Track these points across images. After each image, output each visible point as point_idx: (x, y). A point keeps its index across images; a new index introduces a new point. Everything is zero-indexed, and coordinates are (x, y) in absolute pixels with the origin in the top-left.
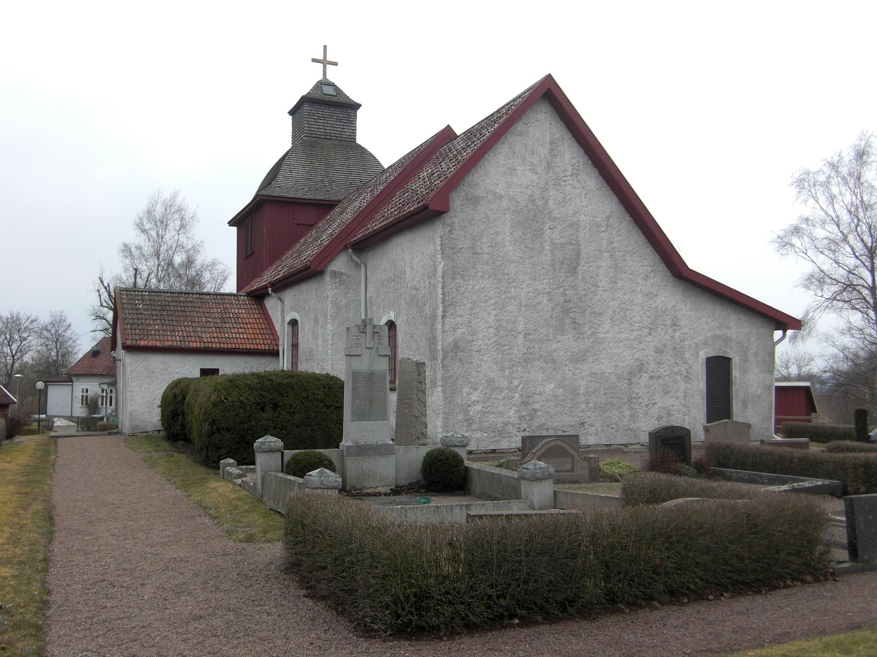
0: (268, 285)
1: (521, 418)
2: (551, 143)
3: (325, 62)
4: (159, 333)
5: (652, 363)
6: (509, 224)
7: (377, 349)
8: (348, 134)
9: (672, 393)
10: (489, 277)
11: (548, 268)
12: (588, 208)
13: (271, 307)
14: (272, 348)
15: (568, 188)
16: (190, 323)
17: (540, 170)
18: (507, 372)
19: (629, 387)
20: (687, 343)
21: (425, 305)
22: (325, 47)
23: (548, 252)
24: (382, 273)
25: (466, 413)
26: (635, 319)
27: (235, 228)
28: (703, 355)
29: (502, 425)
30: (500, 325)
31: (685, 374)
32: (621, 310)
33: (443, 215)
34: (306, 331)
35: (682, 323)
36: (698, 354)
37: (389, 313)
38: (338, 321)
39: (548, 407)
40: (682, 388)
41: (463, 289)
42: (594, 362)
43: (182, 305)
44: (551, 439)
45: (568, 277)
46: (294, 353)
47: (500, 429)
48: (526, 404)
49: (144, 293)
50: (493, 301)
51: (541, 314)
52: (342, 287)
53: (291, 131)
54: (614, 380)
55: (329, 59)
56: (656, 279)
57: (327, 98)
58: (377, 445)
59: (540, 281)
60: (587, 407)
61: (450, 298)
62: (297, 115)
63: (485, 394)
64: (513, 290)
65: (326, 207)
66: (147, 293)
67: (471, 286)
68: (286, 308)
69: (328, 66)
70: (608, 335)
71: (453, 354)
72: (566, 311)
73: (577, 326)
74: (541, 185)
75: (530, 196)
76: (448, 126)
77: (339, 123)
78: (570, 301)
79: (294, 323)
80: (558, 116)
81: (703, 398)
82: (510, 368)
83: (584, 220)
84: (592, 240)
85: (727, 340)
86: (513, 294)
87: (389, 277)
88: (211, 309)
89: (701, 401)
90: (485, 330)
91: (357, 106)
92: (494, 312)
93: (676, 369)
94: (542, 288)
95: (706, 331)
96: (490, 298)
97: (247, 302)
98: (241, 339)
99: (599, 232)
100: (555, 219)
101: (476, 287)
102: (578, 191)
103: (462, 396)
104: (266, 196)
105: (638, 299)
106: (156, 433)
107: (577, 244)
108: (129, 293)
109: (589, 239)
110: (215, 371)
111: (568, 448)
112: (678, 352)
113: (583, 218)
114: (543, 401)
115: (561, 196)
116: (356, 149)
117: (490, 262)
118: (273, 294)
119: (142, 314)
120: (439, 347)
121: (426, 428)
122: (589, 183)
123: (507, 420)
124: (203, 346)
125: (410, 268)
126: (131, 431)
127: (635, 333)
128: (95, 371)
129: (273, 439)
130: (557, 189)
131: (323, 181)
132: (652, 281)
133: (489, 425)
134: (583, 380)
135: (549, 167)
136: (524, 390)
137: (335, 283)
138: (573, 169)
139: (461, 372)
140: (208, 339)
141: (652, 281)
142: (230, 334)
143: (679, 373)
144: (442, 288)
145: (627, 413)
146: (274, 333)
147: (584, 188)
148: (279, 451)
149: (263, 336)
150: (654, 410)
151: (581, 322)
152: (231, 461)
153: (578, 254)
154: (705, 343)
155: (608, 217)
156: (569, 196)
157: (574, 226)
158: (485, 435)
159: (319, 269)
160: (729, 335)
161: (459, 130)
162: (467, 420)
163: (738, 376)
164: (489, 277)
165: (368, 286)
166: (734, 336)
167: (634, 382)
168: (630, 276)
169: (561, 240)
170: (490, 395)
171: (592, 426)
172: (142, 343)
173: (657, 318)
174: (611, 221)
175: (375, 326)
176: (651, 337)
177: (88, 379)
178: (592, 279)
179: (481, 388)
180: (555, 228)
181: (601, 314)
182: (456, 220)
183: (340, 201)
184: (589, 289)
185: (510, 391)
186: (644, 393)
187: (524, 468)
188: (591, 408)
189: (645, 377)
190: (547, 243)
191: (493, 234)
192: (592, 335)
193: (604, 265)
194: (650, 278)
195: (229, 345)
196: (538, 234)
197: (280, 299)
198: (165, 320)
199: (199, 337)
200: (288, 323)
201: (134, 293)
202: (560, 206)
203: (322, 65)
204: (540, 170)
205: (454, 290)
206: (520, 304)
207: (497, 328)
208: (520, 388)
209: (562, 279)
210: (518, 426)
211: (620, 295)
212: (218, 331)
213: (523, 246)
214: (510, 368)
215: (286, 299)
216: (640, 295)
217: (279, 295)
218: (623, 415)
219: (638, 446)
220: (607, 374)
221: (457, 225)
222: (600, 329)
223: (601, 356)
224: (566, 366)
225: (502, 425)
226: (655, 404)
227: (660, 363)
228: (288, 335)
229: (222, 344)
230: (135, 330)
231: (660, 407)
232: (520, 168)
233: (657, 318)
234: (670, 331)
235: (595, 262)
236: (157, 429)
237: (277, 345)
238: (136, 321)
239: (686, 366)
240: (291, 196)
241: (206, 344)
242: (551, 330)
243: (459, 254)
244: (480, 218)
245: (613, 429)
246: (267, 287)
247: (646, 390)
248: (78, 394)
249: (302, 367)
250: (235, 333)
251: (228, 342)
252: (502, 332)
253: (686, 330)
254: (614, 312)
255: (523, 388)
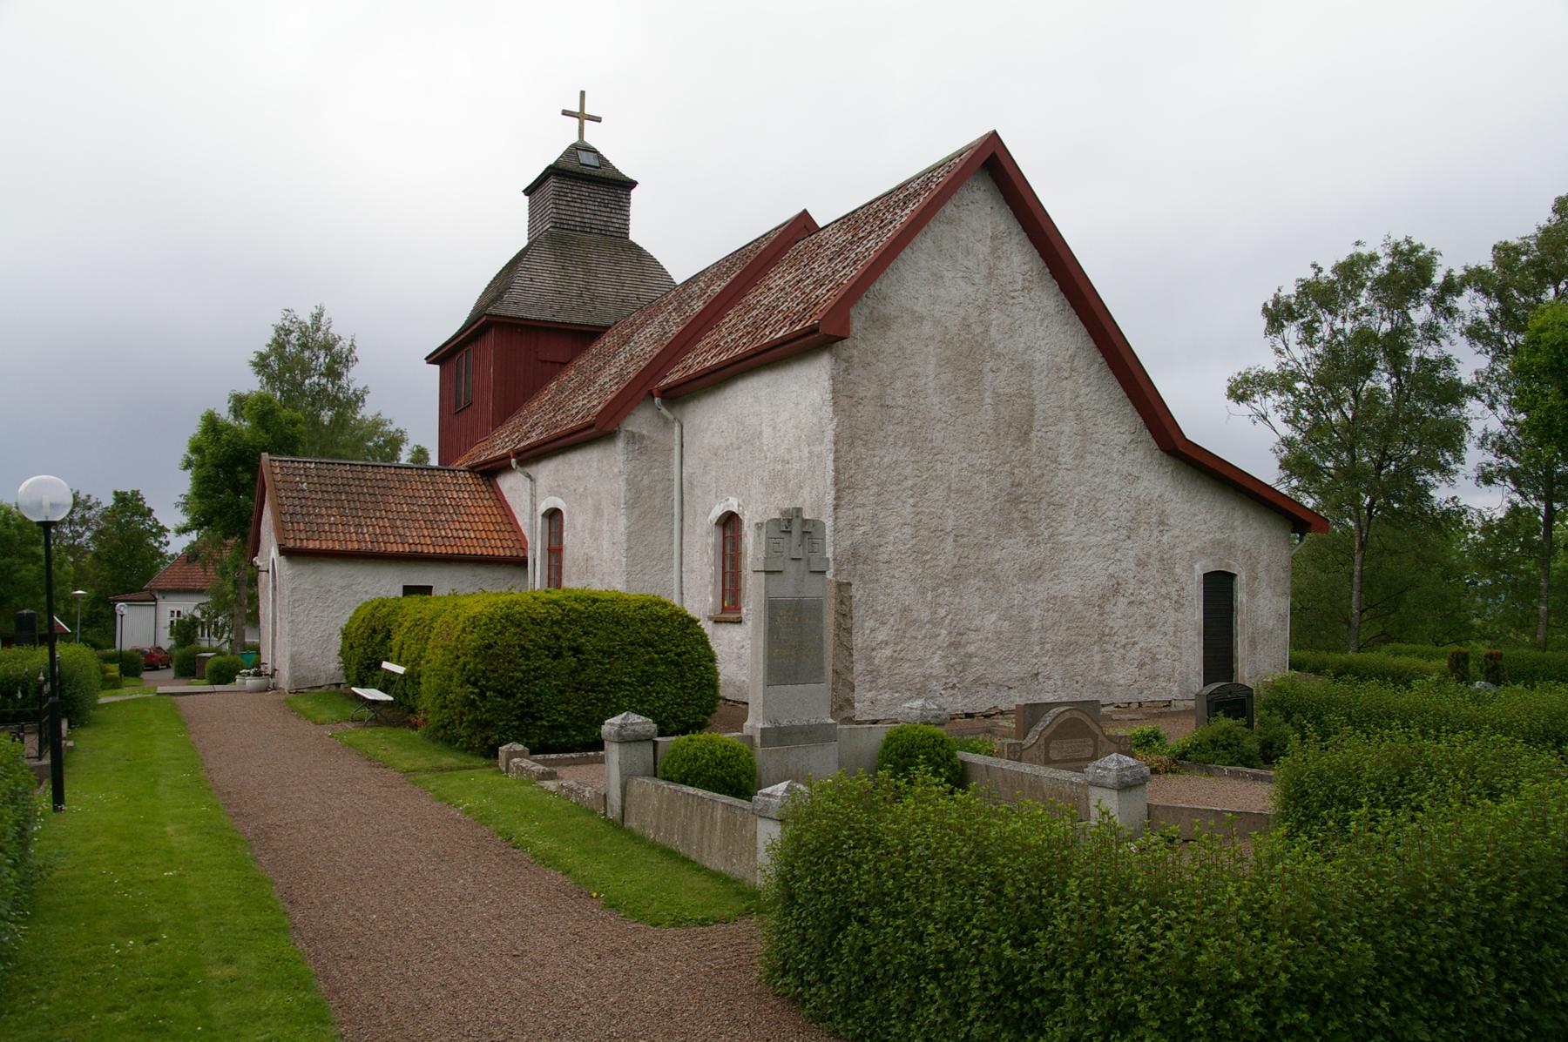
0: (511, 454)
1: (949, 667)
2: (993, 238)
3: (582, 116)
4: (337, 529)
5: (1133, 581)
6: (933, 361)
7: (809, 560)
8: (617, 225)
9: (1158, 628)
10: (904, 446)
11: (990, 432)
12: (1046, 341)
13: (511, 488)
14: (515, 554)
15: (1018, 309)
16: (384, 512)
17: (977, 279)
18: (929, 595)
19: (1099, 618)
20: (1178, 551)
21: (801, 487)
22: (583, 94)
23: (989, 408)
24: (713, 436)
25: (870, 660)
26: (1109, 514)
27: (438, 367)
28: (1199, 570)
29: (922, 679)
30: (920, 521)
31: (1175, 598)
32: (1090, 501)
33: (835, 345)
34: (579, 527)
35: (1172, 521)
36: (1192, 567)
37: (727, 500)
38: (637, 512)
39: (988, 650)
40: (1171, 620)
41: (866, 463)
42: (1052, 580)
43: (369, 484)
44: (1062, 709)
45: (1017, 448)
46: (553, 561)
47: (918, 686)
48: (955, 645)
49: (308, 465)
50: (910, 483)
51: (979, 504)
52: (644, 457)
53: (528, 219)
54: (1080, 607)
55: (588, 111)
56: (1137, 453)
57: (587, 170)
58: (810, 726)
59: (978, 452)
60: (1042, 649)
61: (846, 476)
62: (537, 195)
63: (898, 630)
64: (939, 466)
65: (587, 335)
66: (313, 465)
67: (878, 459)
68: (539, 491)
69: (586, 121)
70: (1072, 538)
71: (850, 567)
72: (1015, 500)
73: (1029, 524)
74: (979, 303)
75: (964, 319)
76: (805, 211)
77: (604, 209)
78: (1020, 485)
79: (554, 515)
80: (1002, 197)
81: (1198, 635)
82: (934, 589)
83: (1040, 360)
84: (1050, 390)
85: (1231, 547)
86: (939, 472)
87: (728, 442)
88: (416, 492)
89: (1196, 640)
90: (897, 529)
91: (633, 184)
92: (911, 501)
93: (1164, 591)
94: (981, 464)
95: (1203, 534)
96: (906, 478)
97: (471, 482)
98: (466, 539)
99: (1061, 379)
100: (999, 355)
101: (886, 460)
102: (1031, 314)
103: (863, 634)
104: (496, 316)
105: (1114, 483)
106: (334, 688)
107: (1030, 396)
108: (285, 464)
109: (1047, 389)
110: (427, 590)
111: (1089, 722)
112: (1166, 565)
113: (1038, 356)
114: (981, 640)
115: (1009, 321)
116: (630, 249)
117: (905, 421)
118: (519, 468)
119: (307, 499)
120: (829, 555)
121: (853, 690)
122: (1046, 302)
123: (929, 671)
124: (407, 550)
125: (770, 429)
126: (294, 686)
127: (1109, 536)
128: (191, 585)
129: (635, 718)
130: (1002, 311)
131: (581, 295)
132: (1132, 457)
133: (902, 680)
134: (1037, 607)
135: (990, 276)
136: (954, 623)
137: (633, 451)
138: (1024, 280)
139: (862, 596)
140: (417, 538)
141: (1132, 457)
142: (448, 531)
143: (1167, 597)
144: (834, 461)
145: (1098, 658)
146: (516, 529)
147: (1039, 310)
148: (649, 739)
149: (500, 534)
150: (1134, 653)
151: (1035, 517)
152: (519, 747)
153: (1032, 411)
154: (1202, 552)
155: (1073, 357)
156: (1018, 322)
157: (1025, 368)
158: (897, 695)
159: (608, 429)
160: (1232, 539)
161: (823, 217)
162: (871, 672)
163: (1244, 600)
164: (904, 446)
165: (685, 456)
166: (1240, 541)
167: (1107, 610)
168: (1103, 449)
169: (1007, 390)
170: (904, 632)
171: (1049, 679)
172: (311, 545)
173: (1138, 512)
174: (1076, 362)
175: (805, 521)
176: (1130, 542)
177: (180, 598)
178: (1051, 452)
179: (892, 621)
180: (998, 370)
181: (1062, 506)
182: (855, 352)
183: (608, 327)
184: (1046, 466)
185: (934, 625)
186: (1121, 627)
187: (1098, 768)
188: (1048, 651)
189: (1123, 602)
190: (988, 394)
191: (910, 377)
192: (1050, 537)
193: (1067, 429)
194: (1130, 452)
195: (298, 541)
196: (975, 378)
197: (529, 476)
198: (345, 509)
199: (400, 536)
200: (543, 515)
201: (292, 465)
202: (1007, 336)
203: (577, 120)
204: (977, 279)
205: (852, 464)
206: (949, 488)
207: (915, 526)
208: (947, 621)
209: (1009, 450)
210: (944, 680)
211: (1089, 476)
212: (429, 526)
213: (953, 397)
214: (934, 589)
215: (540, 476)
216: (1116, 478)
217: (528, 470)
218: (1092, 663)
219: (1112, 708)
220: (1071, 599)
221: (856, 360)
222: (1062, 530)
223: (1062, 571)
224: (1013, 585)
225: (922, 679)
226: (1135, 643)
227: (1142, 582)
228: (542, 533)
229: (437, 547)
230: (299, 523)
231: (1141, 649)
232: (949, 275)
233: (1138, 512)
234: (1156, 533)
235: (1056, 425)
236: (334, 682)
237: (524, 549)
238: (298, 508)
239: (1177, 586)
240: (533, 317)
241: (413, 547)
242: (993, 529)
243: (860, 407)
244: (891, 351)
245: (1077, 682)
246: (509, 457)
247: (1123, 622)
248: (166, 619)
249: (573, 581)
250: (457, 530)
251: (447, 544)
252: (923, 532)
253: (1177, 532)
254: (1080, 502)
255: (952, 620)
